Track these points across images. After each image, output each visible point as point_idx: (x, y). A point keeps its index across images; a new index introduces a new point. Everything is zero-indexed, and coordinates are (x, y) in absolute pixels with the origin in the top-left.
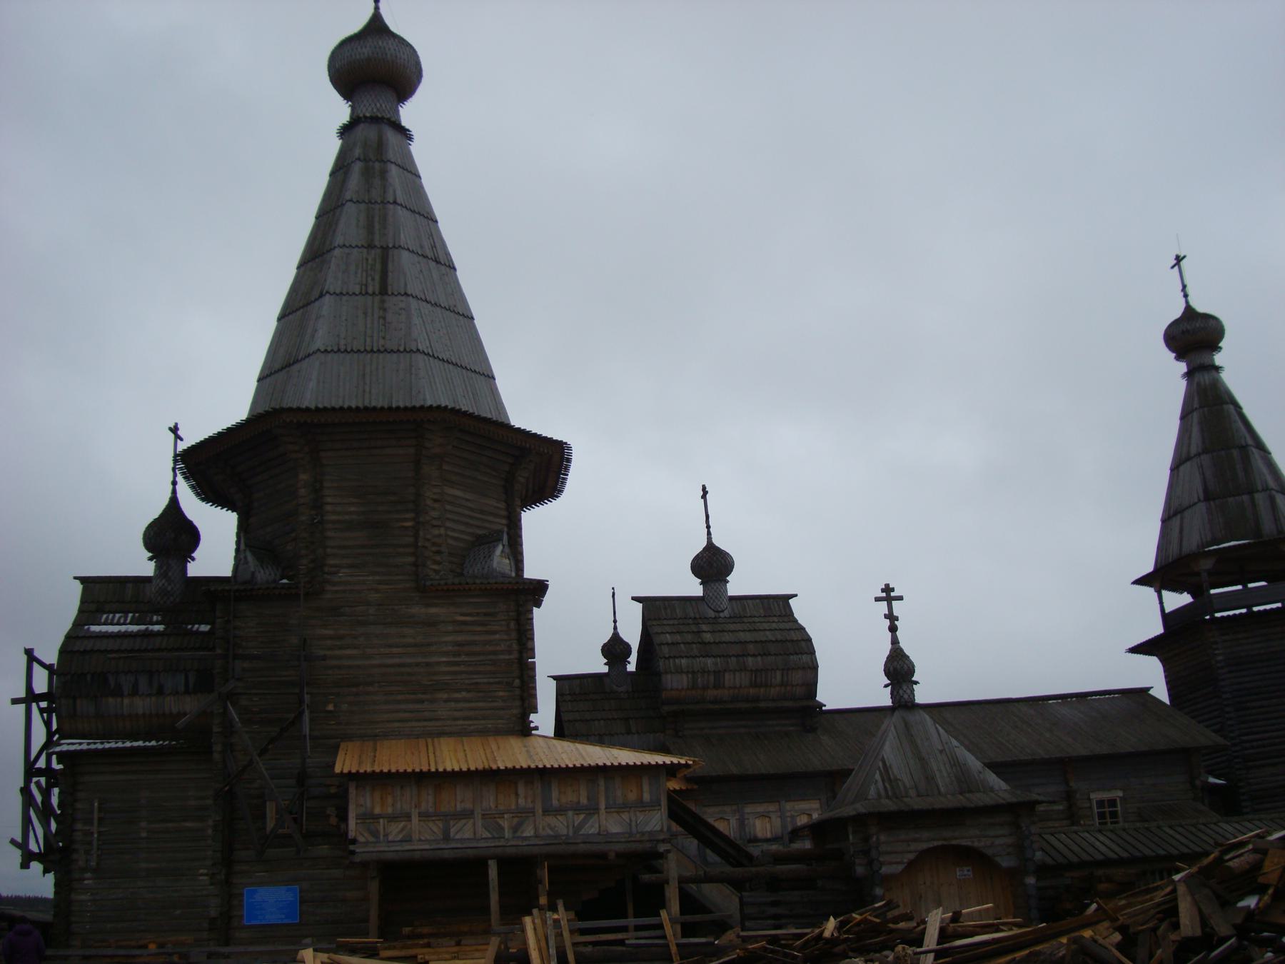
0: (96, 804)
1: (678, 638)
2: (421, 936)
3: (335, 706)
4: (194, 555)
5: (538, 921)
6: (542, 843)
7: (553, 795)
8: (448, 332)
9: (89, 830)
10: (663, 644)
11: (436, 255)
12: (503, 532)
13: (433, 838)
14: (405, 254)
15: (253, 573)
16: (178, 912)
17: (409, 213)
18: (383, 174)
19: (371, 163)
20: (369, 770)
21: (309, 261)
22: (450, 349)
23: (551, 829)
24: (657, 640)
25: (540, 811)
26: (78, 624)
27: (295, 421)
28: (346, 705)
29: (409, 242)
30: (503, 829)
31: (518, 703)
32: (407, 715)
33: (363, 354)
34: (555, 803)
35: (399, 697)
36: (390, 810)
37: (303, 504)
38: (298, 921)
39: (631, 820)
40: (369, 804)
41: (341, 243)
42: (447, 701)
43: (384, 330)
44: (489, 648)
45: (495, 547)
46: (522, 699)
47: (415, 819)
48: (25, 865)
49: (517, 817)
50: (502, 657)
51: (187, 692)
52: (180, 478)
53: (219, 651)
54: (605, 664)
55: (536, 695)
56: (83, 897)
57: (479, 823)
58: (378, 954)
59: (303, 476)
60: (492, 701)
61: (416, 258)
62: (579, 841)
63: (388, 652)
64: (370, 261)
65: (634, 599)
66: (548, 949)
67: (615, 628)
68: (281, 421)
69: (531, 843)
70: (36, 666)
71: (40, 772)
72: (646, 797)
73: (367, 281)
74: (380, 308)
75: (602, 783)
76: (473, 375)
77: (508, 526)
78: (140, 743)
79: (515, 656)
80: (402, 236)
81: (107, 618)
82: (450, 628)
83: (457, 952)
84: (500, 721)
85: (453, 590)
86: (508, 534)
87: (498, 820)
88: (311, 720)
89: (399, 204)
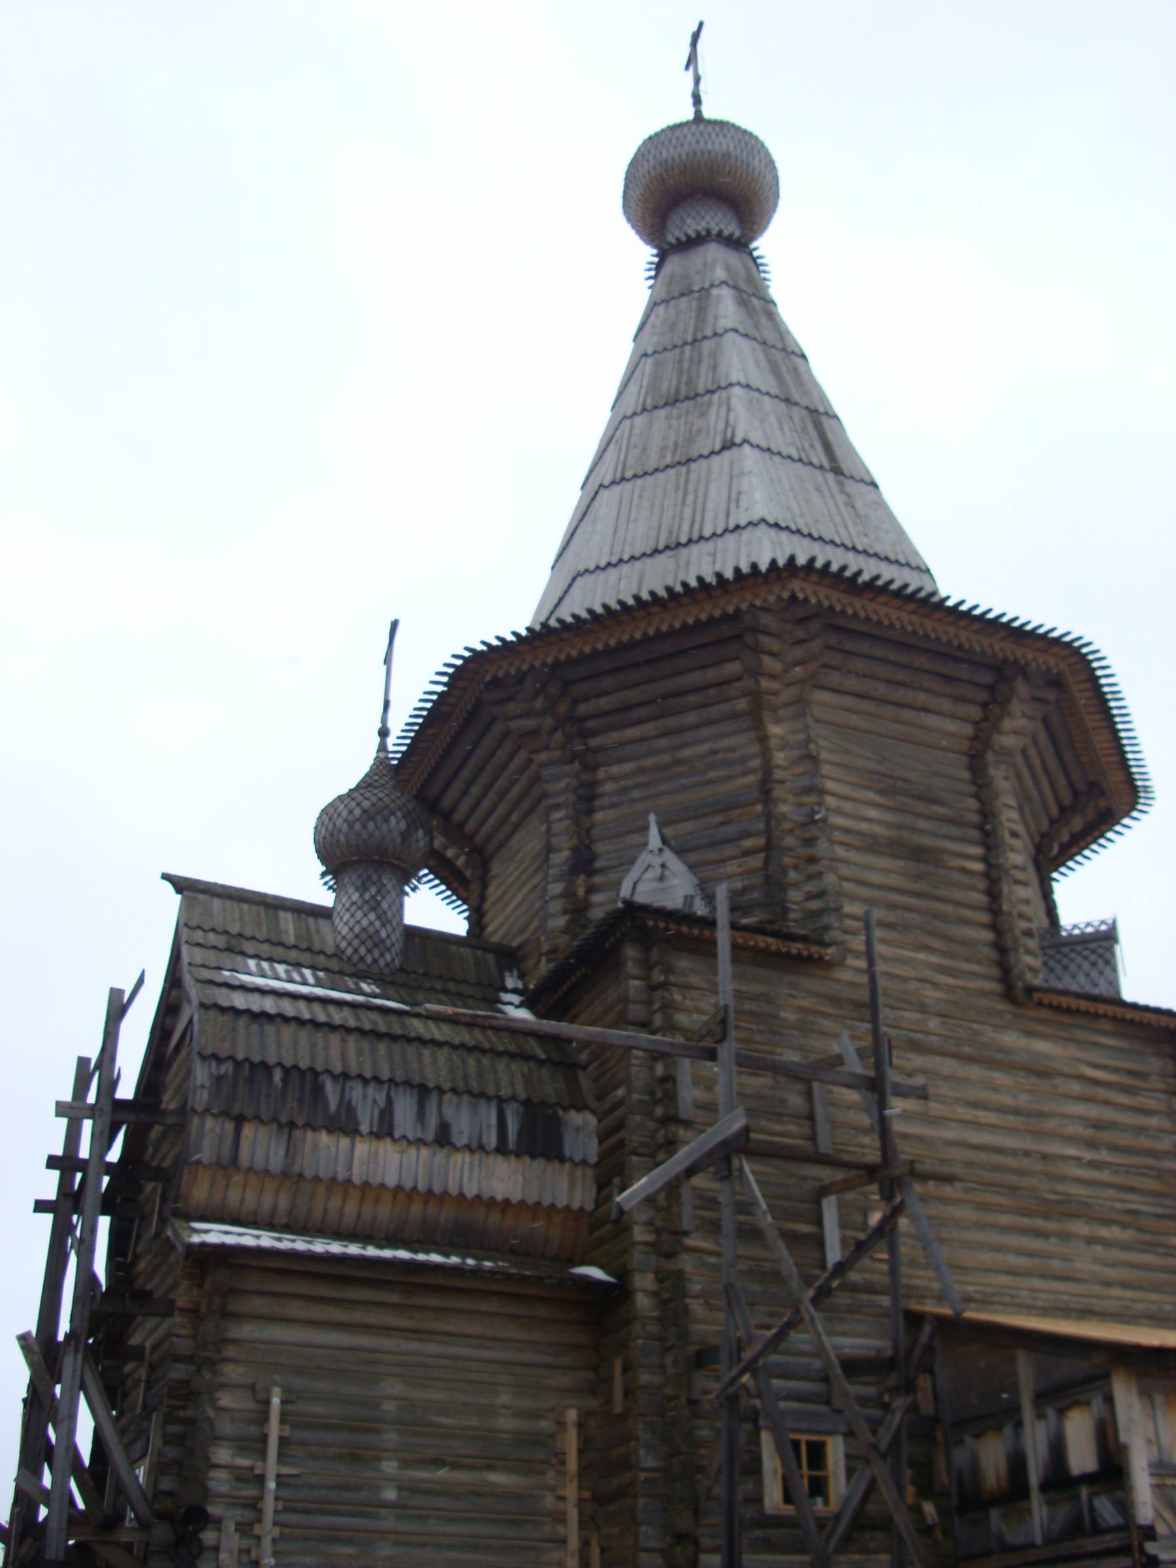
0: (276, 1401)
9: (252, 1468)
35: (1004, 1219)
42: (1090, 1241)
51: (502, 1149)
63: (969, 1117)
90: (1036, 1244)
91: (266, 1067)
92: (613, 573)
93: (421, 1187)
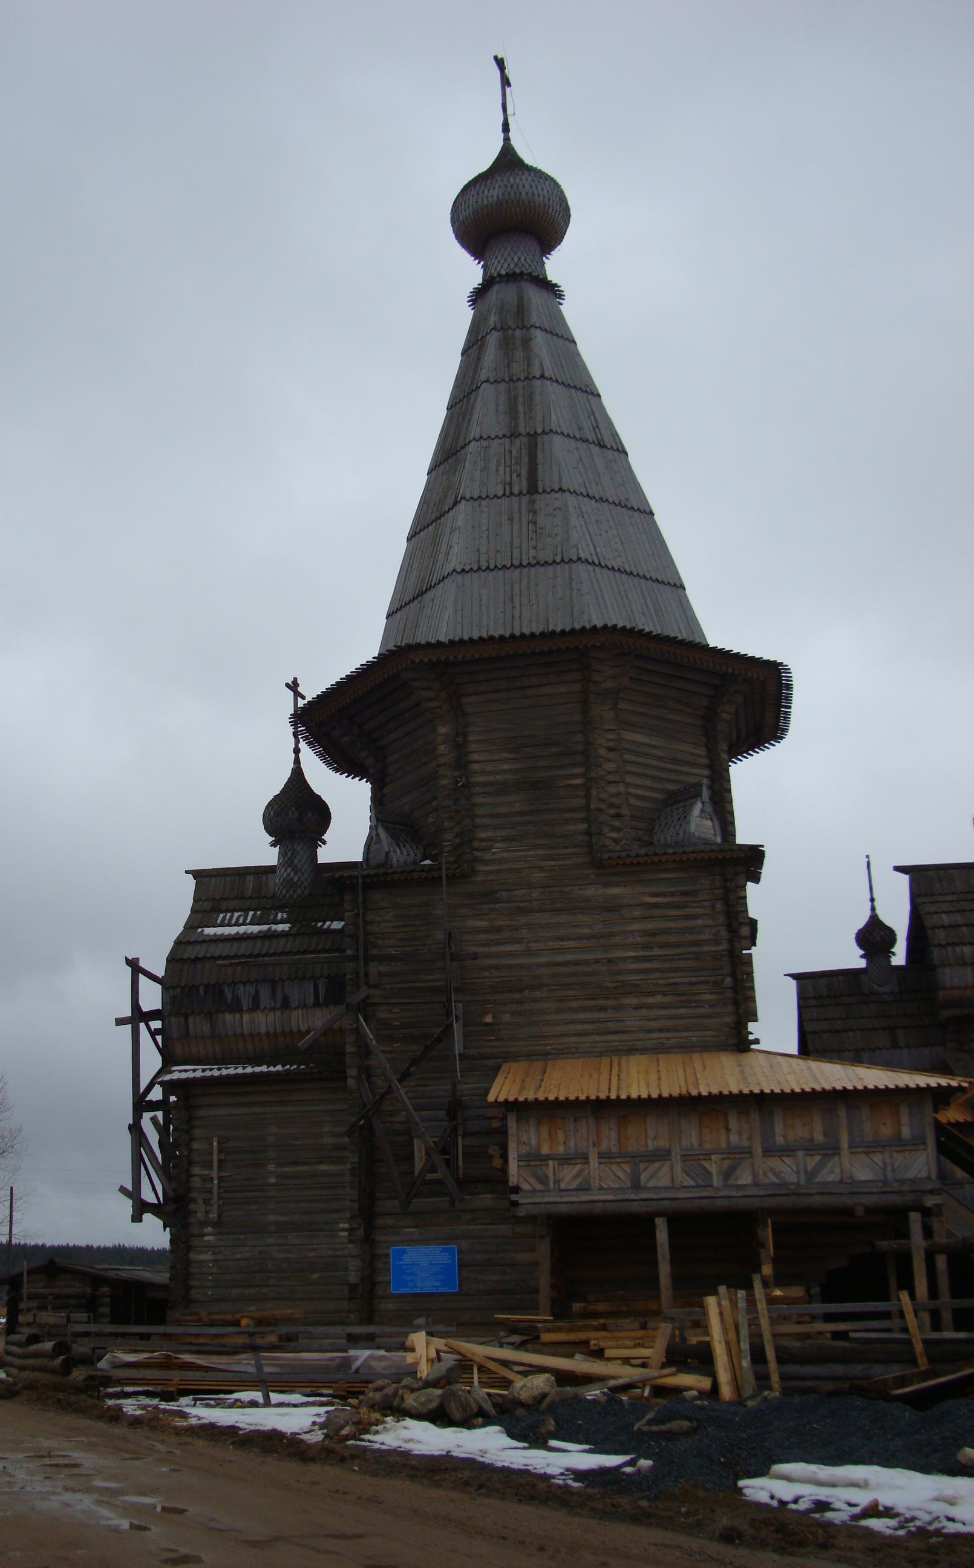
1: (958, 918)
2: (595, 1315)
3: (494, 1017)
4: (324, 837)
5: (725, 1303)
6: (762, 1193)
7: (777, 1130)
8: (618, 534)
9: (209, 1175)
10: (937, 927)
11: (600, 437)
12: (701, 786)
13: (618, 1186)
14: (558, 440)
15: (387, 853)
16: (316, 1276)
17: (561, 388)
18: (527, 342)
19: (510, 332)
20: (531, 1097)
21: (441, 464)
22: (622, 554)
23: (775, 1174)
24: (929, 922)
25: (760, 1150)
26: (190, 927)
27: (426, 660)
28: (508, 1016)
29: (563, 425)
30: (709, 1174)
31: (730, 1009)
32: (587, 1027)
33: (510, 571)
34: (779, 1140)
35: (575, 1004)
36: (561, 1149)
37: (445, 765)
38: (457, 1290)
39: (885, 1164)
40: (534, 1142)
41: (477, 436)
43: (534, 538)
44: (689, 937)
45: (692, 805)
46: (736, 1003)
47: (594, 1161)
48: (137, 1218)
49: (729, 1158)
50: (706, 948)
51: (317, 1004)
52: (303, 745)
53: (349, 952)
54: (862, 957)
55: (754, 998)
56: (203, 1257)
57: (678, 1167)
58: (538, 1337)
59: (442, 730)
60: (696, 1007)
61: (573, 444)
62: (812, 1191)
63: (558, 947)
64: (514, 453)
65: (897, 869)
66: (739, 1342)
67: (873, 909)
68: (409, 662)
69: (750, 1193)
70: (142, 979)
71: (153, 1106)
72: (906, 1132)
73: (511, 479)
74: (530, 511)
75: (842, 1112)
76: (654, 585)
77: (710, 778)
78: (264, 1068)
79: (724, 946)
80: (553, 417)
81: (224, 917)
82: (637, 913)
83: (641, 1338)
84: (709, 1033)
85: (639, 863)
86: (710, 788)
87: (703, 1162)
88: (466, 1036)
89: (547, 378)
90: (597, 1015)
91: (196, 988)
92: (399, 613)
93: (272, 1031)
